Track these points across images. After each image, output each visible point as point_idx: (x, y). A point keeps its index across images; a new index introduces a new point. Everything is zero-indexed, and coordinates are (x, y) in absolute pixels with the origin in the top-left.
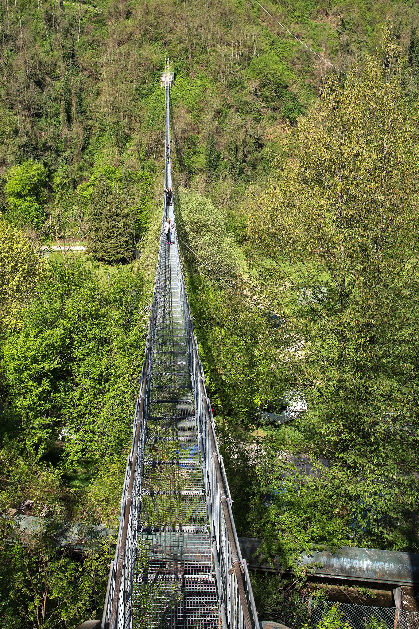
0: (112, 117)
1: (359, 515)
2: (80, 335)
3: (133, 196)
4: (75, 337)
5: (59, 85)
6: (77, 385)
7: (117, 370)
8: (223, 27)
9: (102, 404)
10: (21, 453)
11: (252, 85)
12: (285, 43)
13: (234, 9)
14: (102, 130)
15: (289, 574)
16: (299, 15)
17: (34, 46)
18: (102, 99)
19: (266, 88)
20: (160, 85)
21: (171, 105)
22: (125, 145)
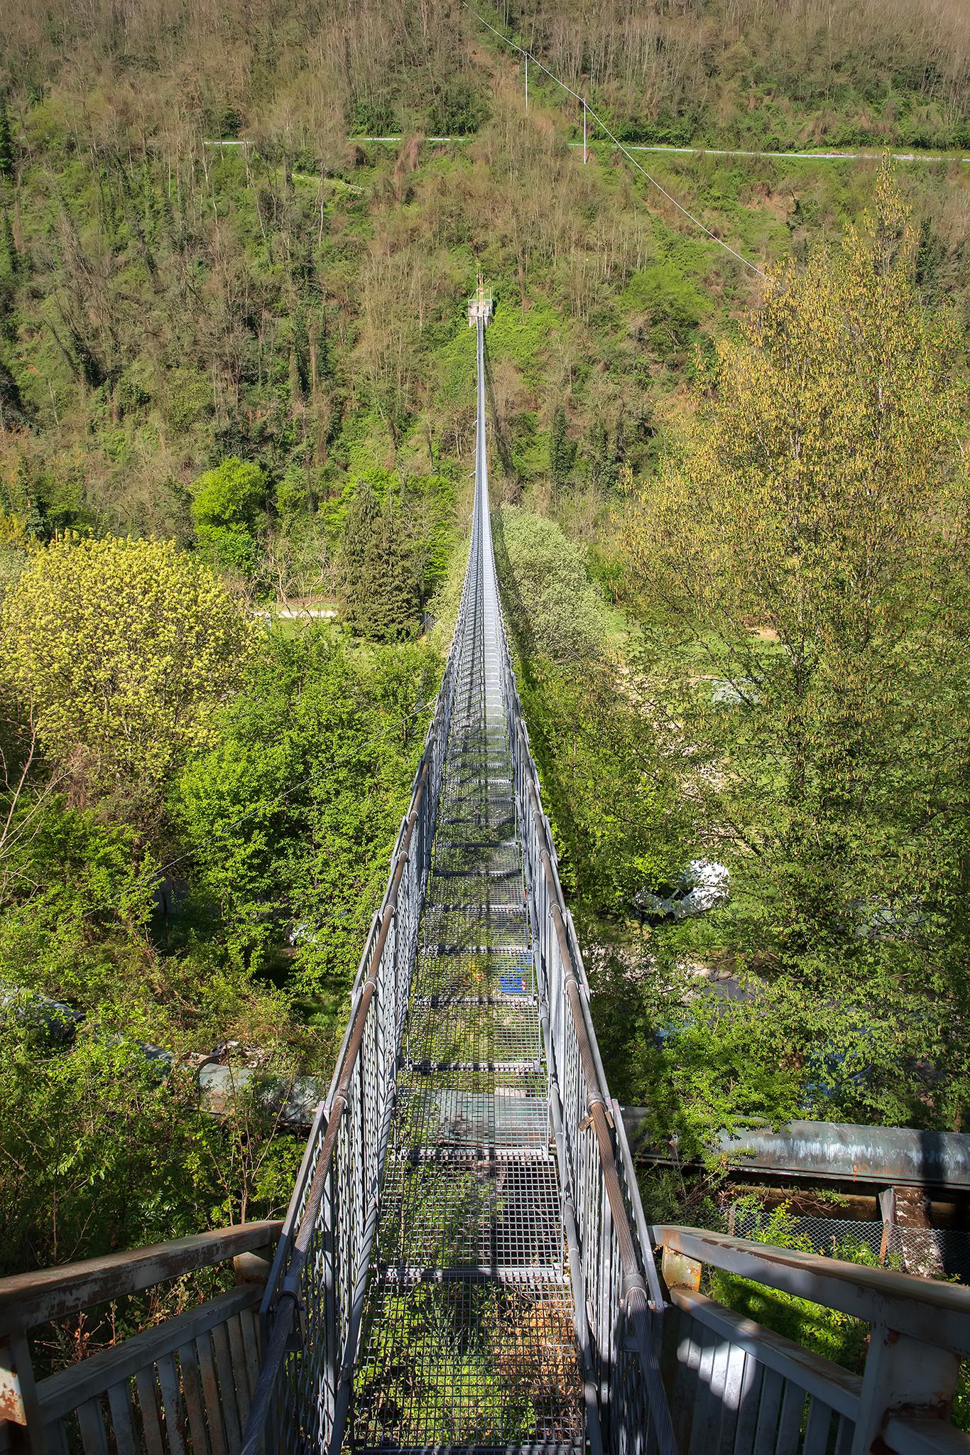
0: (382, 381)
1: (824, 1066)
2: (322, 757)
3: (419, 521)
4: (311, 760)
5: (285, 325)
6: (318, 846)
7: (389, 820)
8: (581, 217)
9: (362, 880)
10: (221, 965)
11: (635, 321)
12: (693, 246)
13: (600, 184)
14: (364, 405)
15: (694, 1169)
16: (718, 194)
17: (240, 255)
18: (362, 350)
19: (659, 326)
20: (467, 323)
21: (487, 359)
22: (406, 431)
